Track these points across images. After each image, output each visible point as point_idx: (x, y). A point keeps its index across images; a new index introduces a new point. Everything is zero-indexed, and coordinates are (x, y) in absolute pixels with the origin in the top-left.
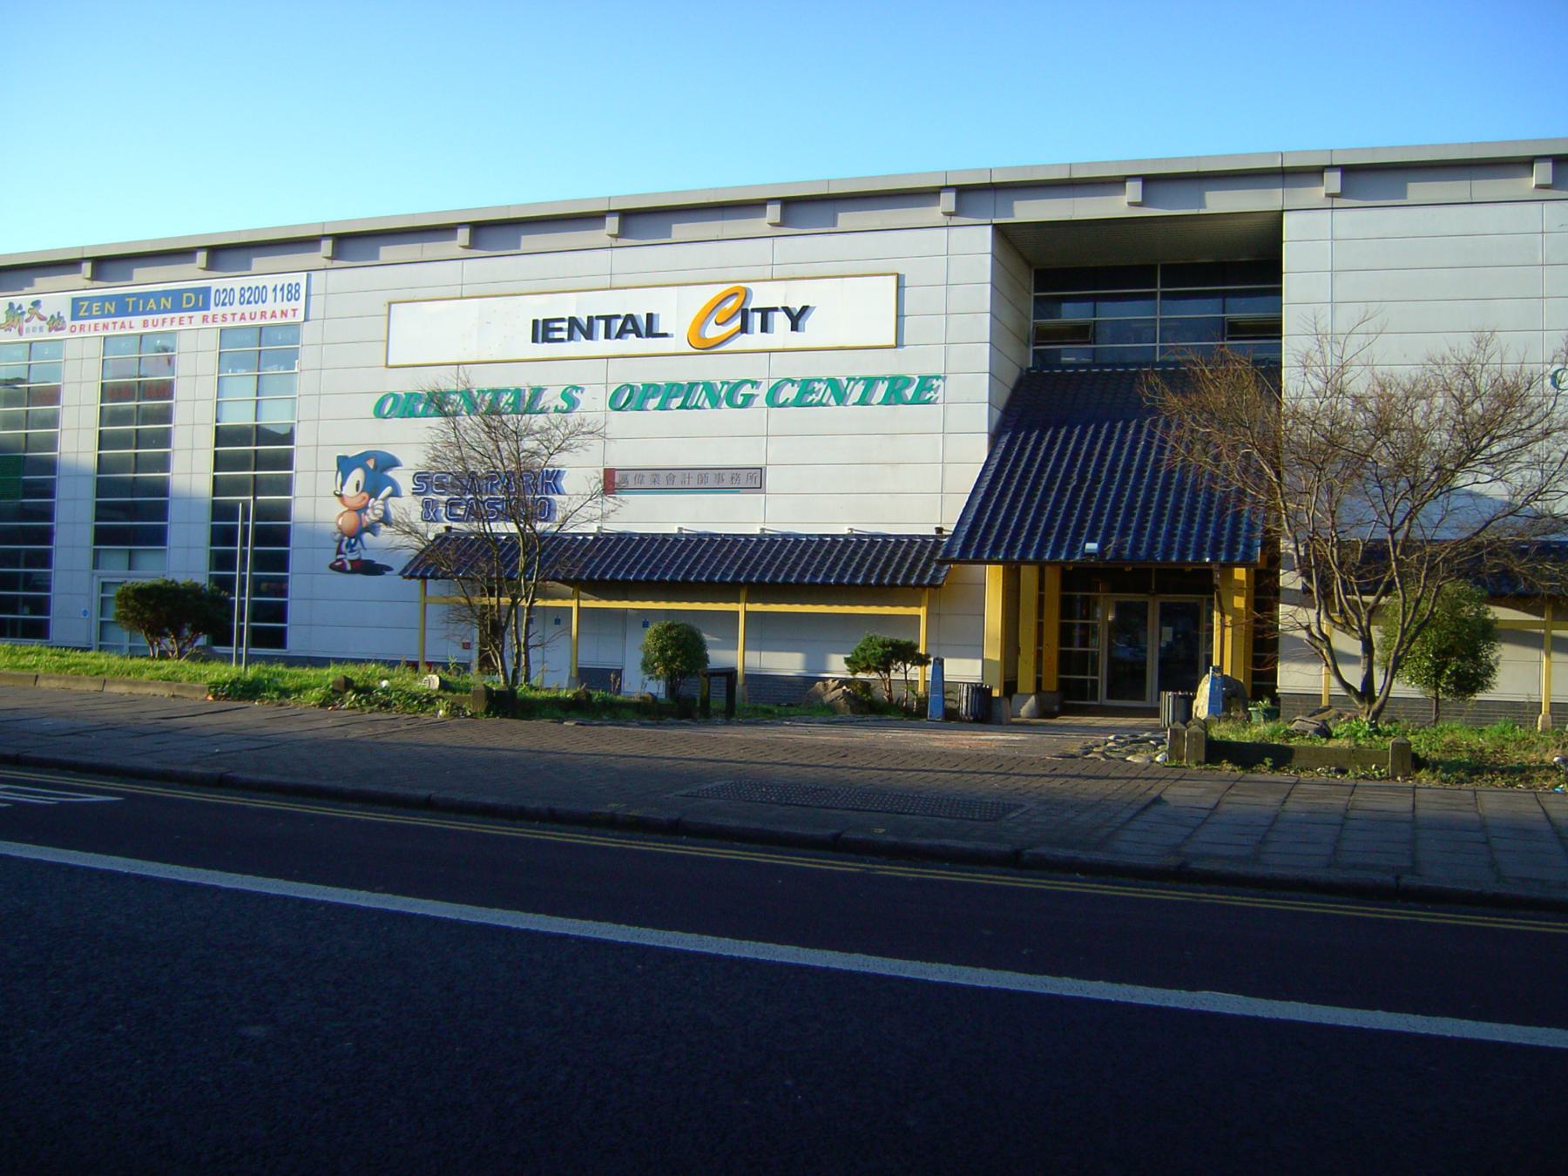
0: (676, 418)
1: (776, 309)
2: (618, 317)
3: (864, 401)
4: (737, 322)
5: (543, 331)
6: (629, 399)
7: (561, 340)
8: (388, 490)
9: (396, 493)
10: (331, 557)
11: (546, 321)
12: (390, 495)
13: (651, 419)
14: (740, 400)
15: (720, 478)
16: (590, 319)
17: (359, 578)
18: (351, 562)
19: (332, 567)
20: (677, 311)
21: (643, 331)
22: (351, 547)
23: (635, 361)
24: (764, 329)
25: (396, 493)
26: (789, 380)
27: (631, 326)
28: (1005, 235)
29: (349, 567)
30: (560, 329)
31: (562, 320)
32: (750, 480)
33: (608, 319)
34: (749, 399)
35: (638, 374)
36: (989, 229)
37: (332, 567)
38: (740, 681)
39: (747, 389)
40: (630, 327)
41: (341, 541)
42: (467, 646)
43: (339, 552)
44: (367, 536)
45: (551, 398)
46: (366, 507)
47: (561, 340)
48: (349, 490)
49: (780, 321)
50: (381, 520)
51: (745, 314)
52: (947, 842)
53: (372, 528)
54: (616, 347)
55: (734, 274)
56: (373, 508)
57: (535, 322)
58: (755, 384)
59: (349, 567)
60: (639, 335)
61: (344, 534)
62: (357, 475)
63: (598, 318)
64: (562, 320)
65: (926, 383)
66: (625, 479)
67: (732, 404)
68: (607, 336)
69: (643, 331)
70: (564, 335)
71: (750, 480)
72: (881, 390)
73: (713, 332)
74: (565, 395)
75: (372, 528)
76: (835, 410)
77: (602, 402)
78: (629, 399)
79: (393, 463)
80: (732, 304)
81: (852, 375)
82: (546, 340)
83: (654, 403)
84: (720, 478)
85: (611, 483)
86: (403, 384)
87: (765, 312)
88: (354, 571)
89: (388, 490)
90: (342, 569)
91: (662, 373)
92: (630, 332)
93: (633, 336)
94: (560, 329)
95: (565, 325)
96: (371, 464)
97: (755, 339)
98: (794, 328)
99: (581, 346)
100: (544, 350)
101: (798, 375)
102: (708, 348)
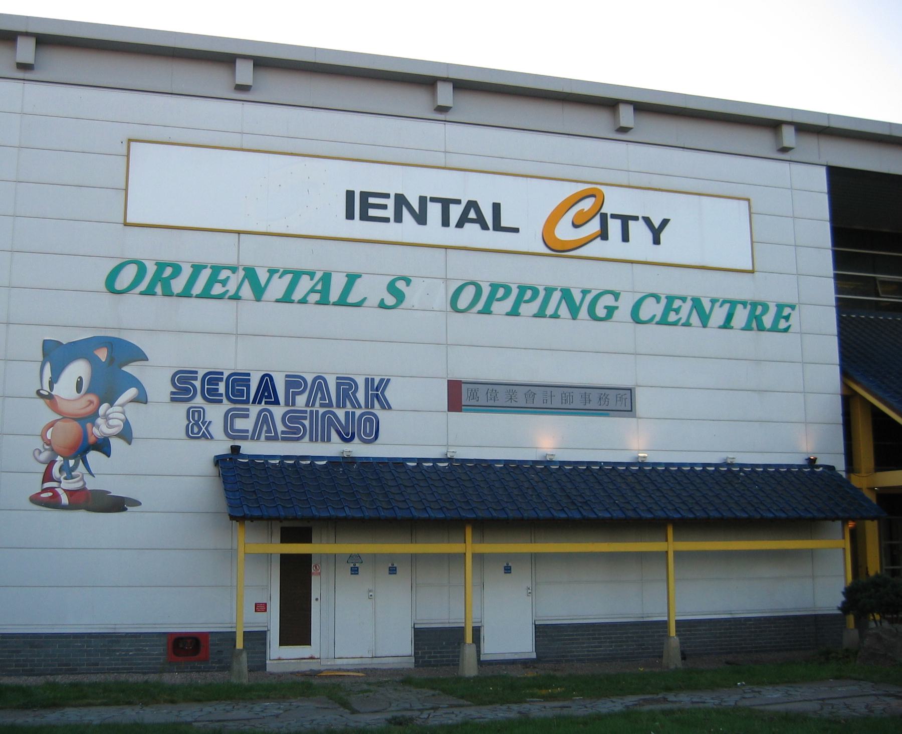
0: (526, 326)
1: (636, 218)
2: (458, 202)
3: (727, 325)
4: (594, 226)
5: (359, 205)
6: (484, 298)
7: (387, 220)
8: (132, 392)
9: (142, 399)
10: (35, 485)
11: (365, 195)
12: (134, 400)
13: (498, 324)
14: (601, 312)
15: (586, 399)
16: (423, 200)
17: (81, 516)
18: (70, 493)
19: (36, 500)
20: (529, 205)
21: (490, 223)
22: (68, 472)
23: (479, 256)
24: (625, 238)
25: (142, 399)
26: (653, 295)
27: (472, 214)
28: (839, 178)
29: (65, 500)
30: (384, 207)
31: (387, 196)
32: (616, 402)
33: (446, 203)
34: (611, 310)
35: (489, 271)
36: (822, 173)
37: (36, 500)
38: (673, 632)
39: (608, 300)
40: (472, 215)
41: (51, 463)
42: (261, 607)
43: (48, 476)
44: (93, 456)
45: (371, 288)
46: (95, 414)
47: (387, 220)
48: (65, 388)
49: (637, 229)
50: (119, 435)
51: (604, 219)
52: (123, 677)
53: (103, 446)
54: (452, 235)
55: (586, 174)
56: (106, 417)
57: (350, 195)
58: (616, 295)
59: (65, 500)
60: (485, 227)
61: (55, 453)
62: (79, 369)
63: (433, 200)
64: (387, 196)
65: (783, 312)
66: (474, 395)
67: (594, 317)
68: (446, 222)
69: (490, 223)
70: (390, 213)
71: (616, 402)
72: (741, 316)
73: (565, 232)
74: (392, 288)
75: (103, 446)
76: (696, 331)
77: (441, 299)
78: (484, 298)
79: (138, 355)
80: (587, 205)
81: (714, 295)
82: (364, 217)
83: (502, 307)
84: (586, 399)
85: (458, 396)
86: (150, 249)
87: (625, 220)
88: (72, 507)
89: (132, 392)
90: (53, 503)
91: (513, 273)
92: (472, 221)
93: (477, 227)
94: (384, 207)
95: (390, 203)
96: (102, 354)
97: (613, 246)
98: (657, 241)
99: (408, 228)
100: (359, 228)
101: (664, 290)
102: (559, 250)
